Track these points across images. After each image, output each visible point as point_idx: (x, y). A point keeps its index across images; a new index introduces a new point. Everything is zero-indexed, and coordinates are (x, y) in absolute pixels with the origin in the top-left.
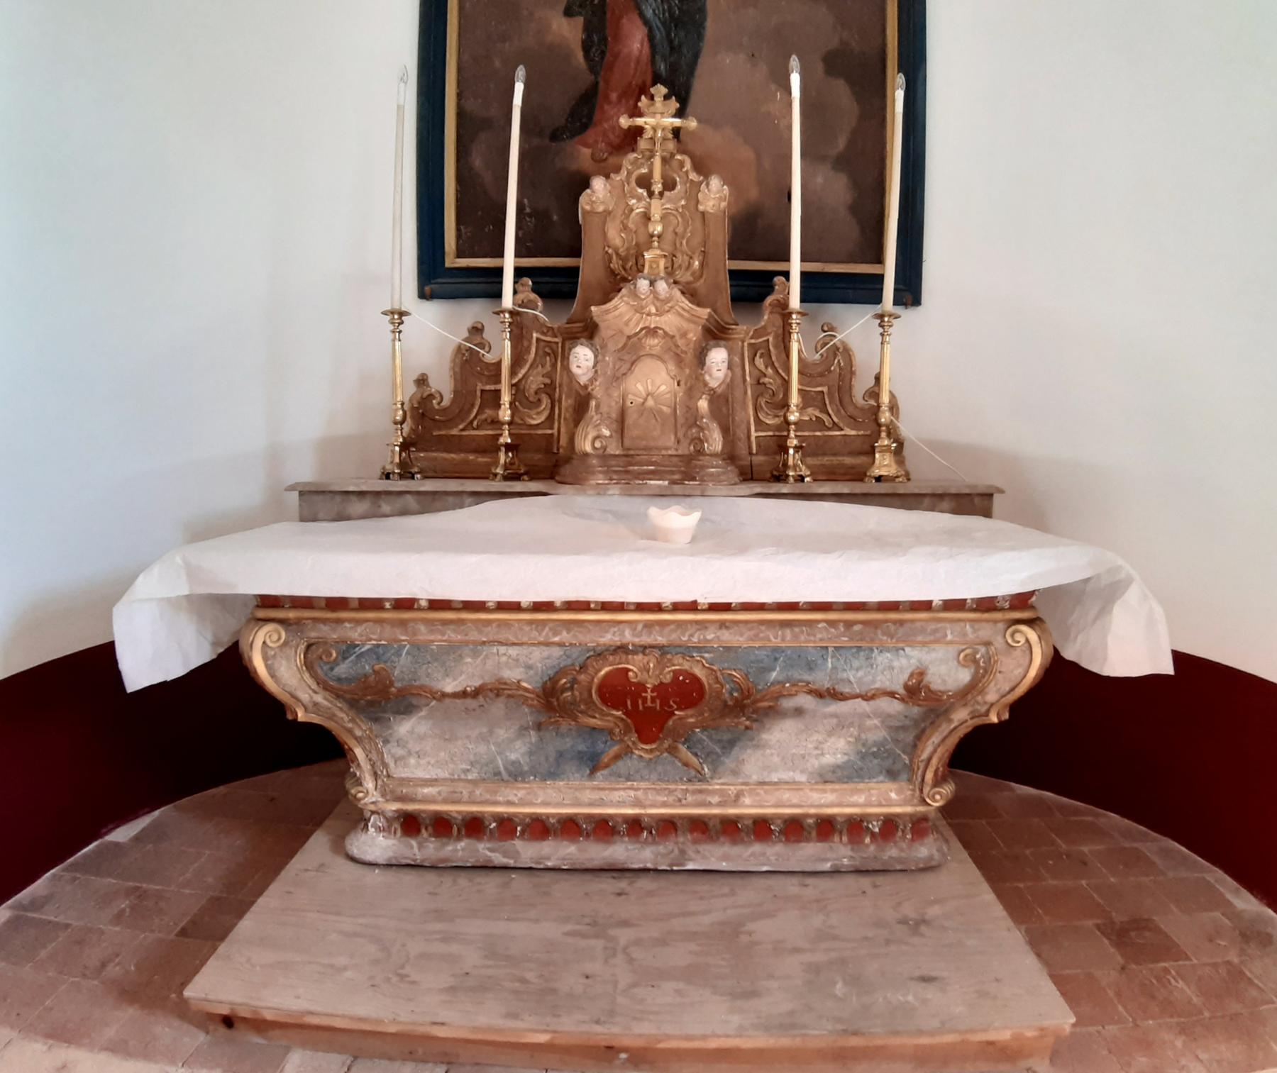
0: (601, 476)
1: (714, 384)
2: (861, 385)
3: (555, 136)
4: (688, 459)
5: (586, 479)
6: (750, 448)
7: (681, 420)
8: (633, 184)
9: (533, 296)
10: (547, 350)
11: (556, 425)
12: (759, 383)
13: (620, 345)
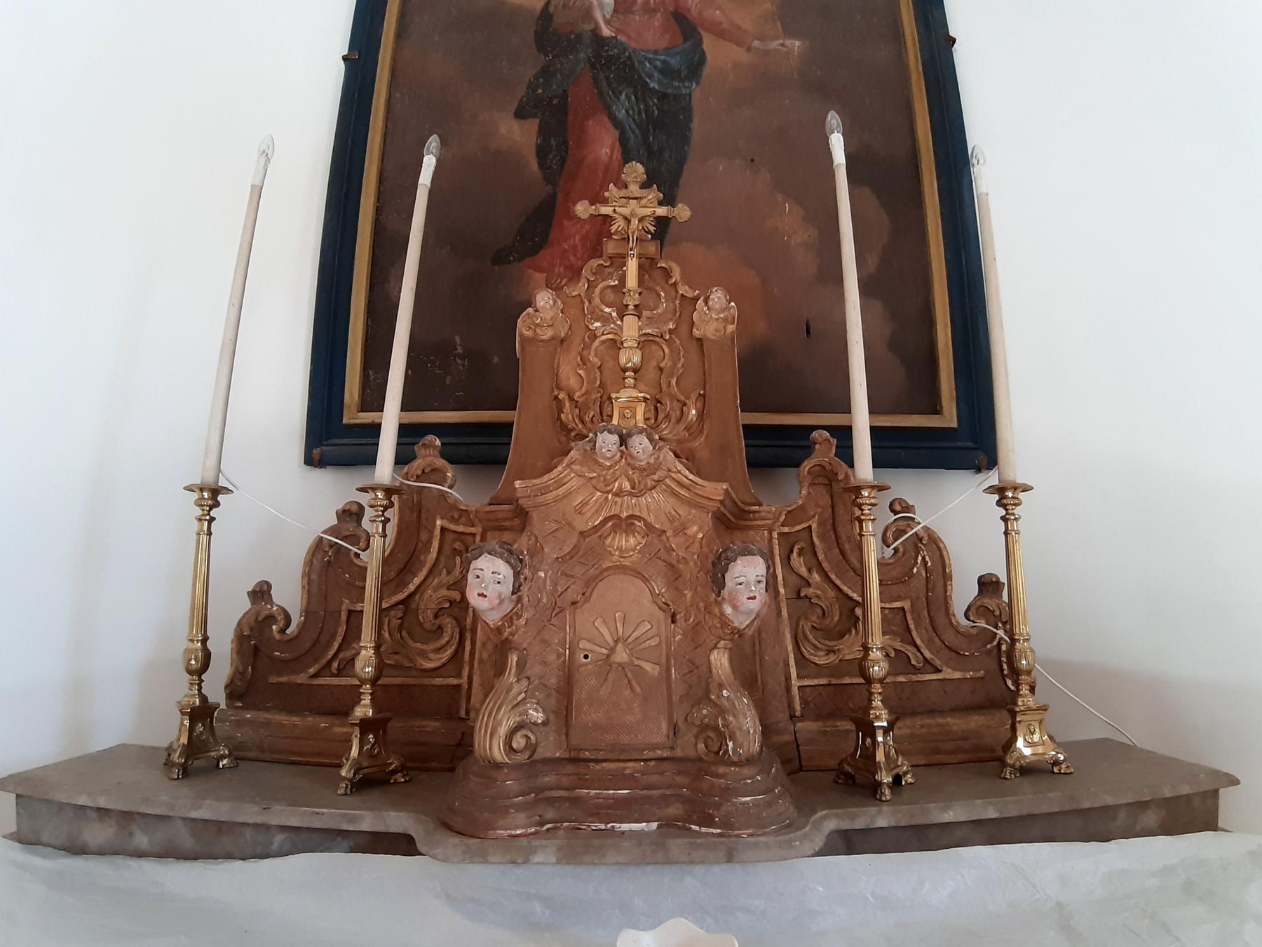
0: (521, 817)
1: (741, 622)
2: (963, 592)
3: (500, 258)
4: (696, 767)
5: (491, 826)
6: (790, 705)
7: (678, 689)
8: (597, 301)
9: (440, 462)
10: (457, 545)
11: (465, 673)
12: (799, 597)
13: (567, 549)
